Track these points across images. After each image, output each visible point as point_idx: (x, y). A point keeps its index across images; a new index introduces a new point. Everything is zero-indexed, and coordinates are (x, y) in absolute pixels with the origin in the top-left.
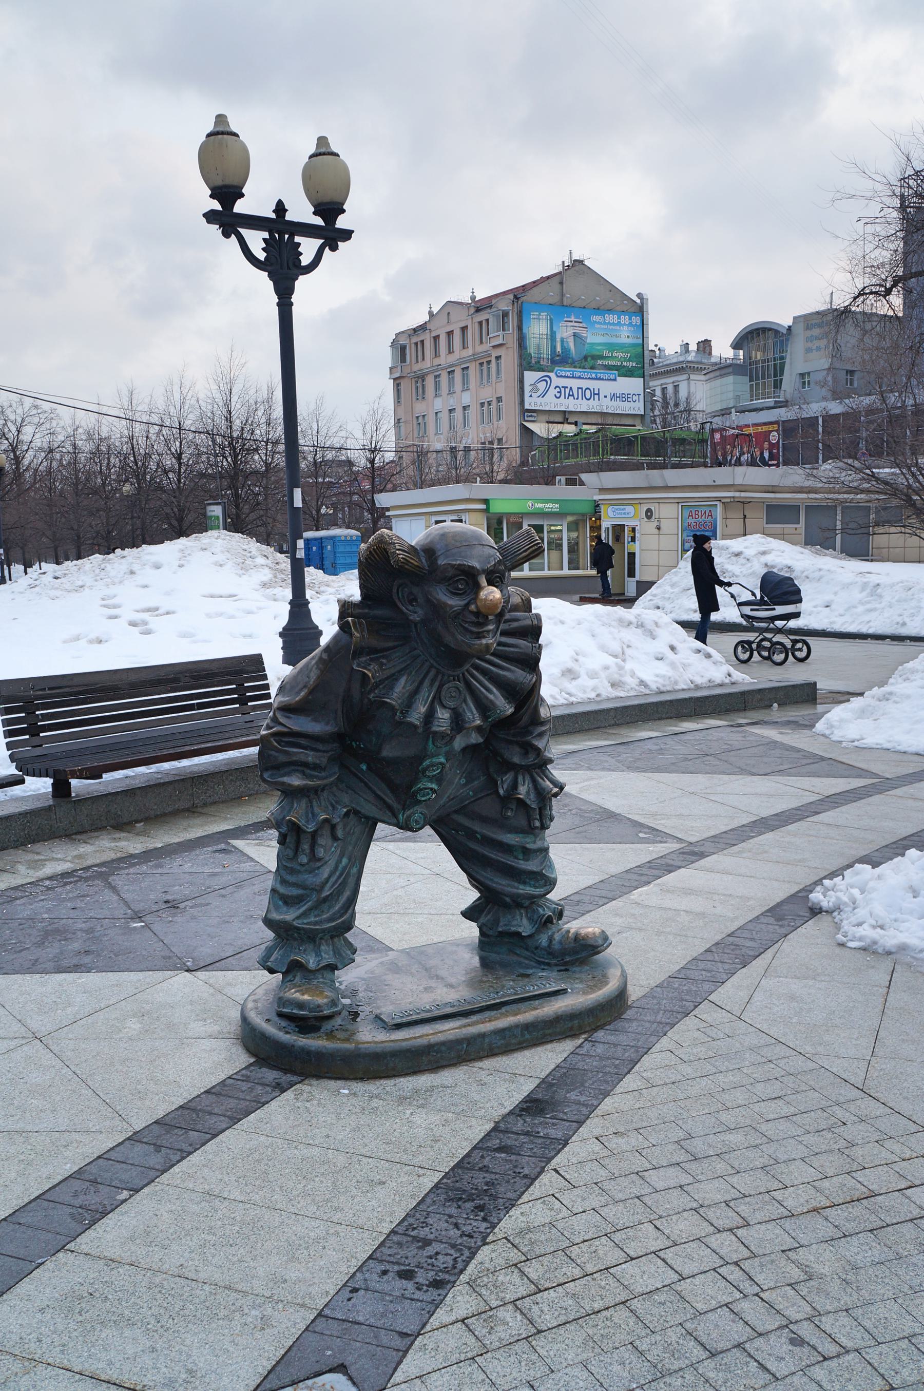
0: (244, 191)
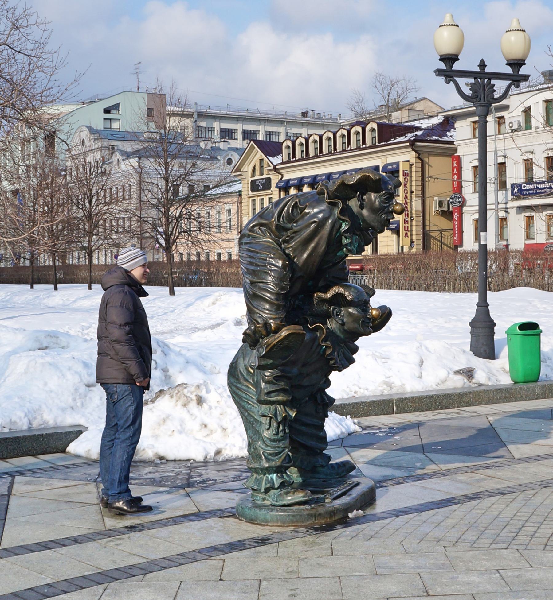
0: (459, 57)
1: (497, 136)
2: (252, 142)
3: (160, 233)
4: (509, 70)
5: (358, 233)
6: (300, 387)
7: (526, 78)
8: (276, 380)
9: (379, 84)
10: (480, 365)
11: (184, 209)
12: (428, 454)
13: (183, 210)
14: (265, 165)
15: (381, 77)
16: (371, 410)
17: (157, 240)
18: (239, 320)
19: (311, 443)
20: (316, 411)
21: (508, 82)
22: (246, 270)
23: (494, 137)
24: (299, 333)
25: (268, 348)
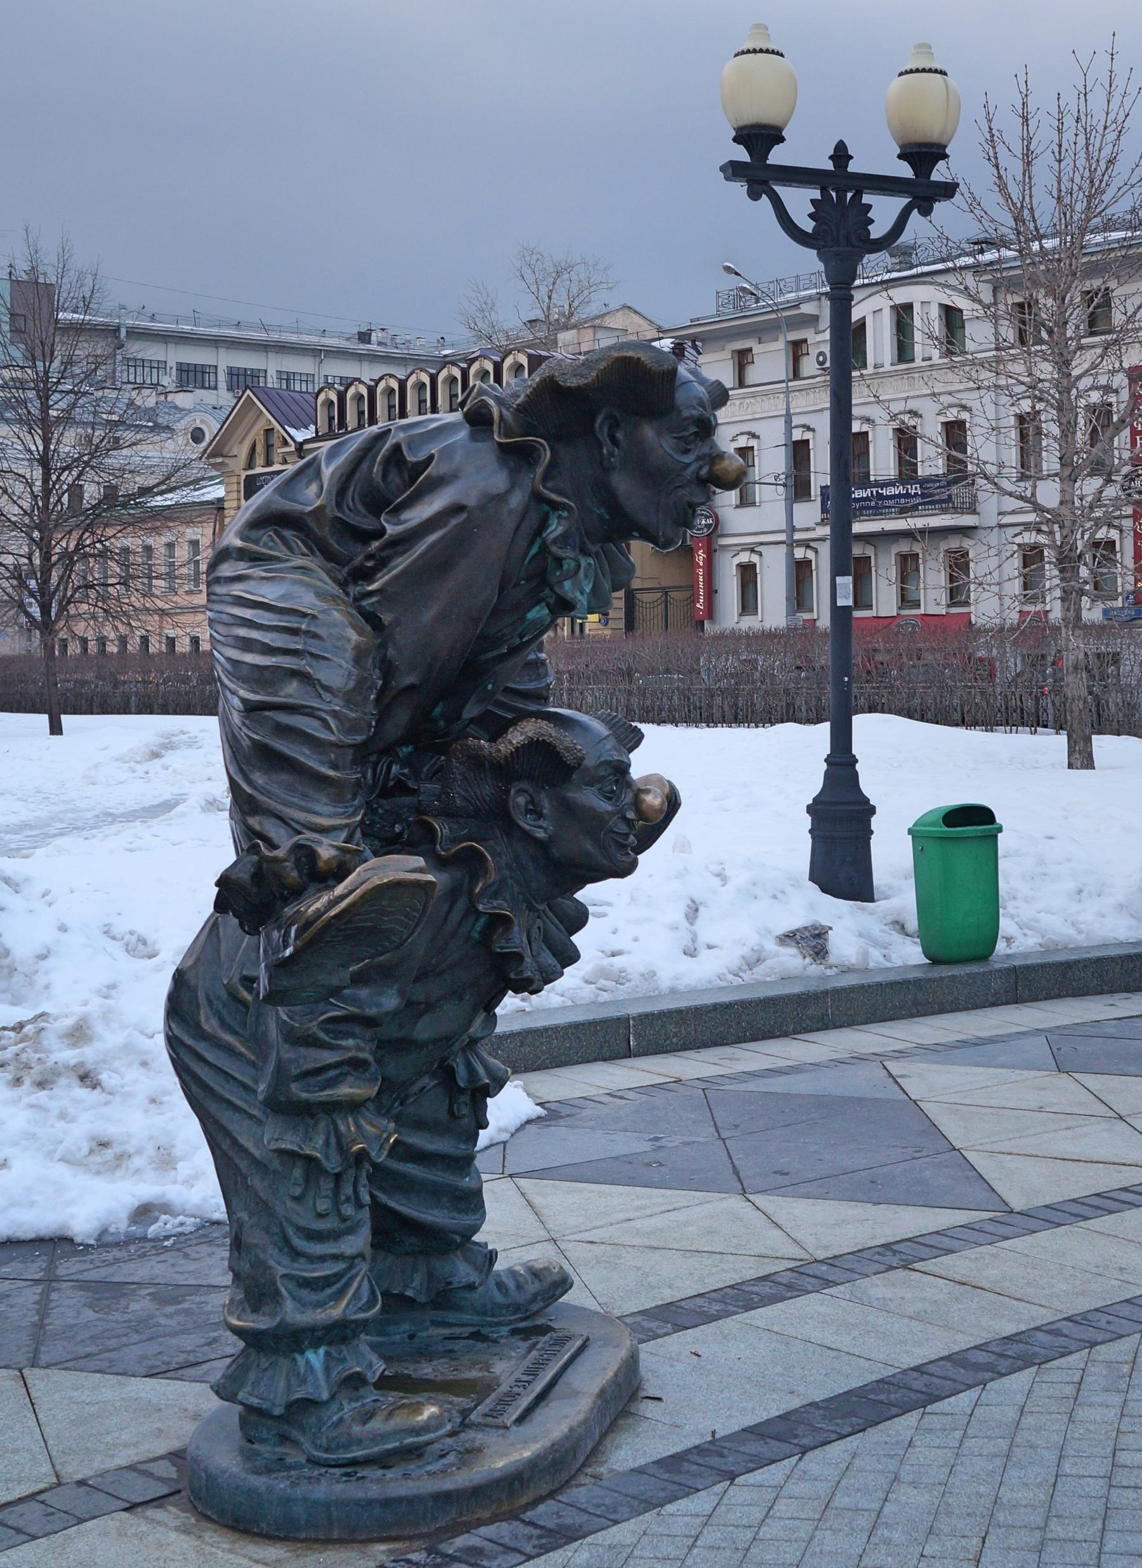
1: (790, 384)
2: (248, 392)
3: (32, 594)
4: (905, 171)
5: (594, 548)
6: (403, 1045)
7: (948, 190)
8: (327, 1032)
9: (530, 271)
10: (841, 917)
11: (87, 534)
12: (758, 1199)
13: (85, 536)
14: (276, 442)
15: (534, 257)
16: (570, 1048)
17: (21, 606)
18: (210, 799)
19: (435, 1216)
20: (451, 1112)
21: (902, 202)
22: (228, 666)
23: (784, 385)
24: (417, 884)
25: (307, 935)
